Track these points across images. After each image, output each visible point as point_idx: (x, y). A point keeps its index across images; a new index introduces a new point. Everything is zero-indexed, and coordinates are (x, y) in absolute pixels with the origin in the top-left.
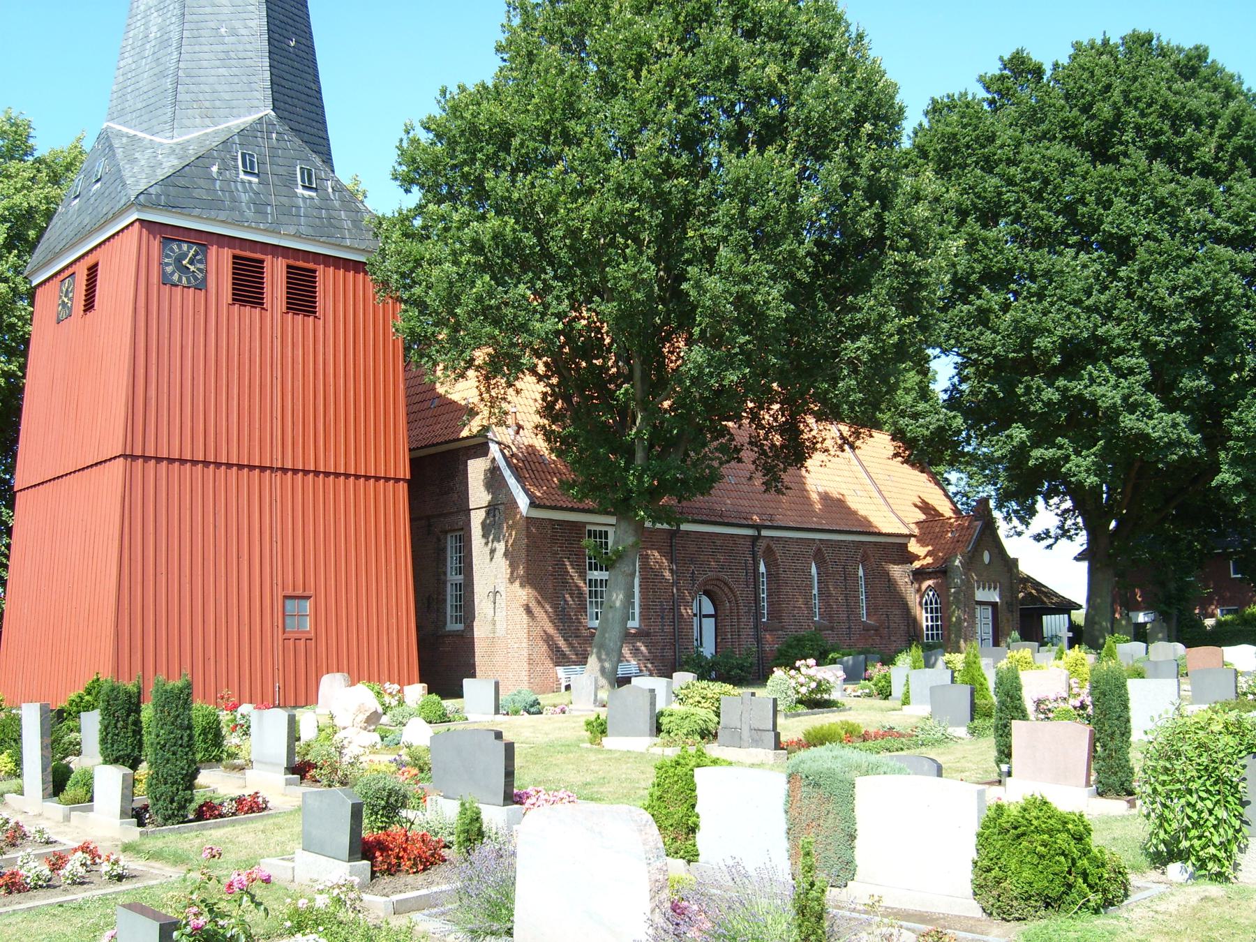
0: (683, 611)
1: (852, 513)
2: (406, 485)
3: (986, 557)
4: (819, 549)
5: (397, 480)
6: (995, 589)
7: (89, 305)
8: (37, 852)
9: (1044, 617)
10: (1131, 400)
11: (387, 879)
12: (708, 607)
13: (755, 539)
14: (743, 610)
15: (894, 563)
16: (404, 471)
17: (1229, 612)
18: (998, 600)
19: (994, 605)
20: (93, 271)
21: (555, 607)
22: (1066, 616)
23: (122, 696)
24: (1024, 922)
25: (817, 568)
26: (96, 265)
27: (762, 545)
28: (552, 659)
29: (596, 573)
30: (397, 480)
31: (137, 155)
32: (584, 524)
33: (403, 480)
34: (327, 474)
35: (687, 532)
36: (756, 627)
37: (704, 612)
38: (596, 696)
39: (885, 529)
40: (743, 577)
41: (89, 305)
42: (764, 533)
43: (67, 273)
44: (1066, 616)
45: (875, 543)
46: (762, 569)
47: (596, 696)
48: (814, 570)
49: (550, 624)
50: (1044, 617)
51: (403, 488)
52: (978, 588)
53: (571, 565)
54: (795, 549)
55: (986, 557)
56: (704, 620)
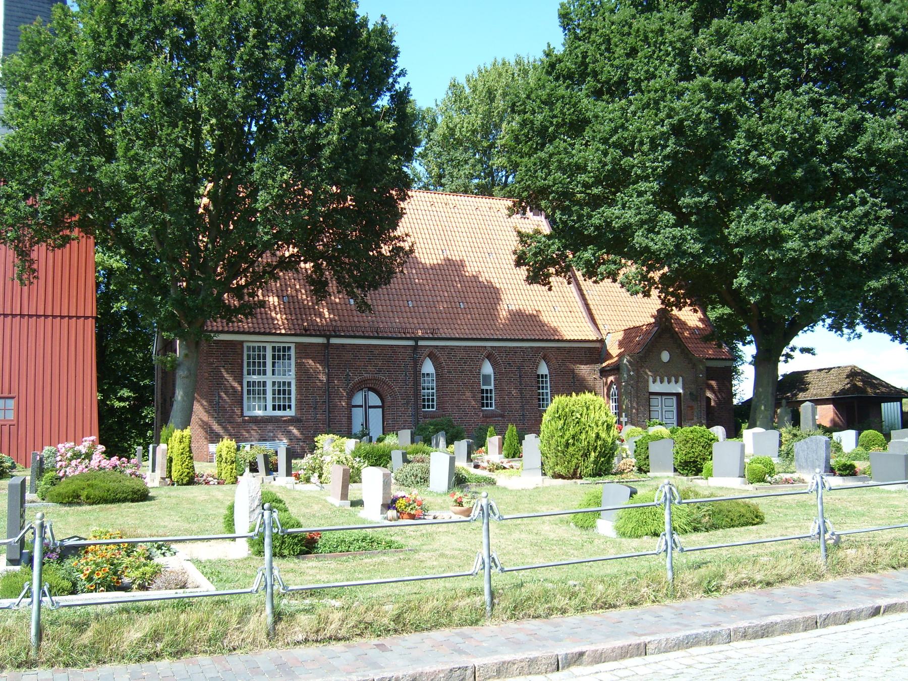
0: (117, 404)
1: (542, 325)
2: (94, 320)
5: (86, 318)
6: (676, 382)
9: (882, 404)
10: (819, 146)
12: (374, 399)
13: (416, 347)
15: (581, 363)
16: (91, 309)
17: (647, 374)
18: (681, 391)
19: (678, 395)
21: (210, 402)
22: (899, 403)
23: (760, 418)
28: (206, 438)
29: (254, 377)
30: (86, 318)
32: (242, 342)
33: (92, 317)
34: (30, 316)
39: (568, 336)
44: (899, 403)
45: (558, 348)
49: (205, 414)
50: (882, 404)
51: (90, 324)
52: (654, 382)
53: (227, 371)
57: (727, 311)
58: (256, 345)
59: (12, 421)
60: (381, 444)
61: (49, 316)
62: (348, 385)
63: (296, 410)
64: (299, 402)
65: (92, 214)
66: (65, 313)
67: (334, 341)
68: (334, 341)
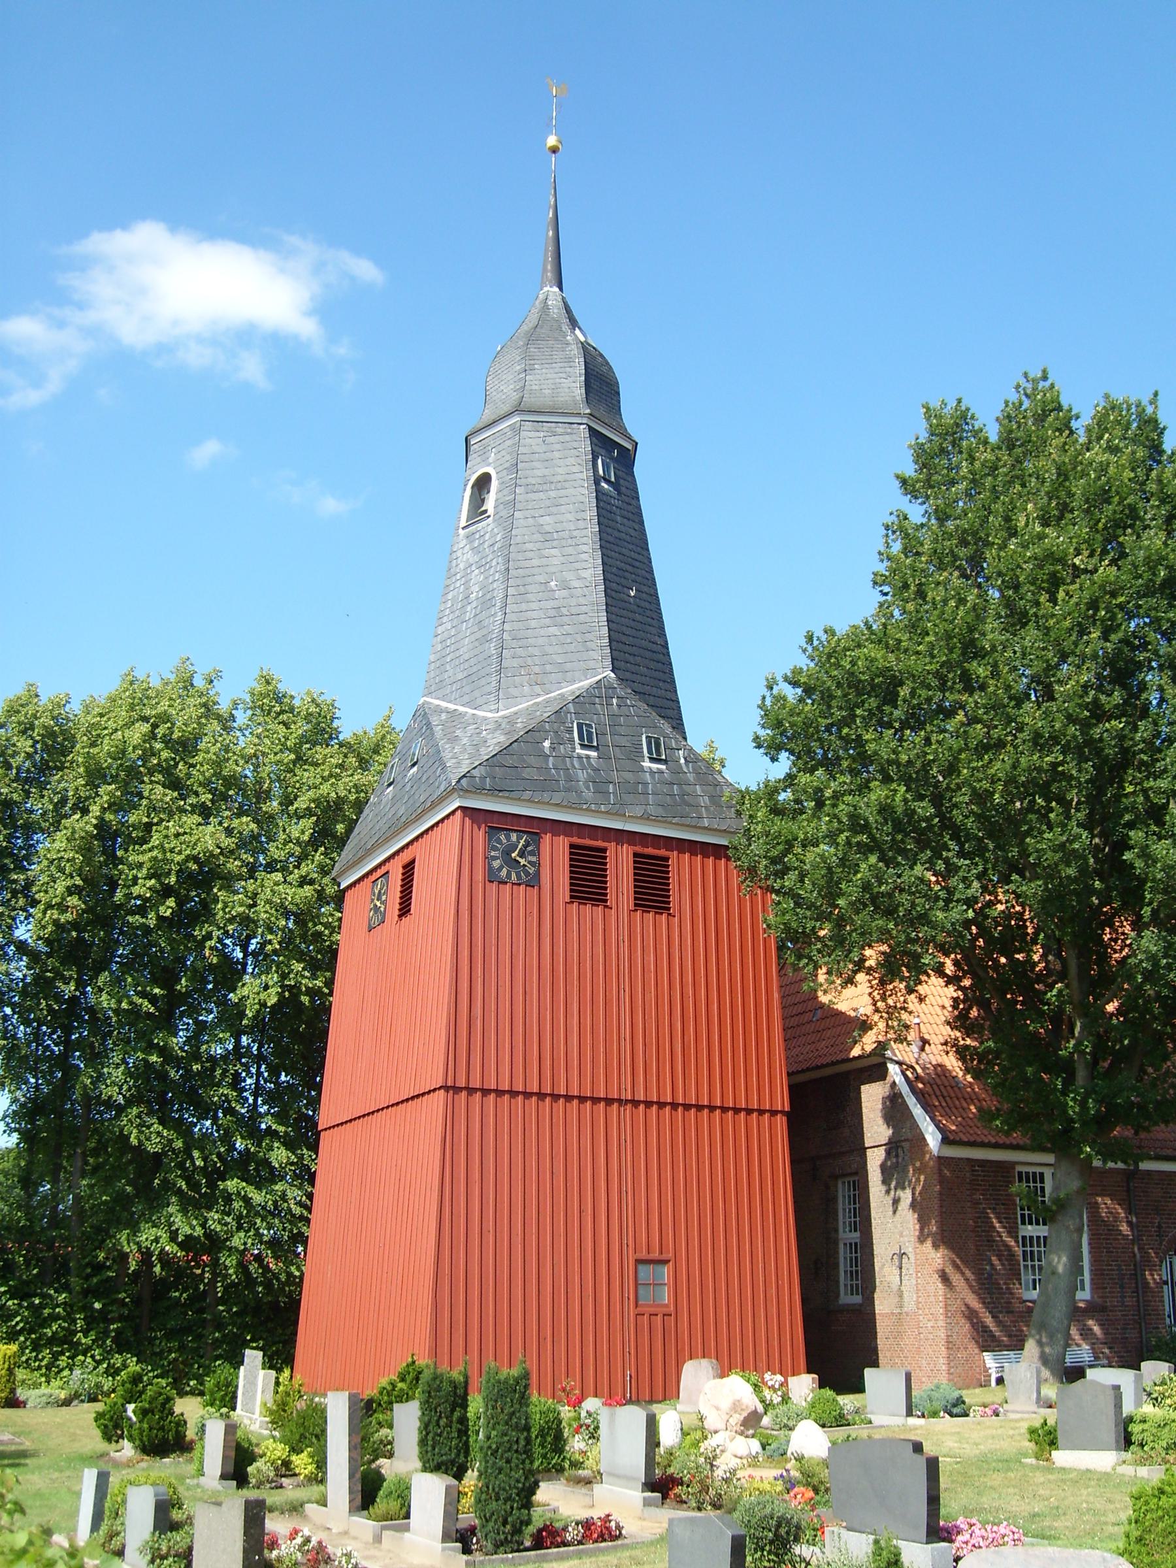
2: (785, 1119)
5: (773, 1113)
16: (782, 1101)
21: (979, 1273)
30: (773, 1113)
32: (1013, 1164)
33: (781, 1112)
51: (781, 1122)
57: (856, 1052)
58: (1031, 1169)
59: (666, 1306)
60: (118, 1454)
61: (461, 1089)
62: (1160, 1244)
63: (1092, 1289)
64: (1097, 1273)
65: (1119, 1011)
66: (462, 1083)
67: (1145, 1166)
68: (1145, 1166)
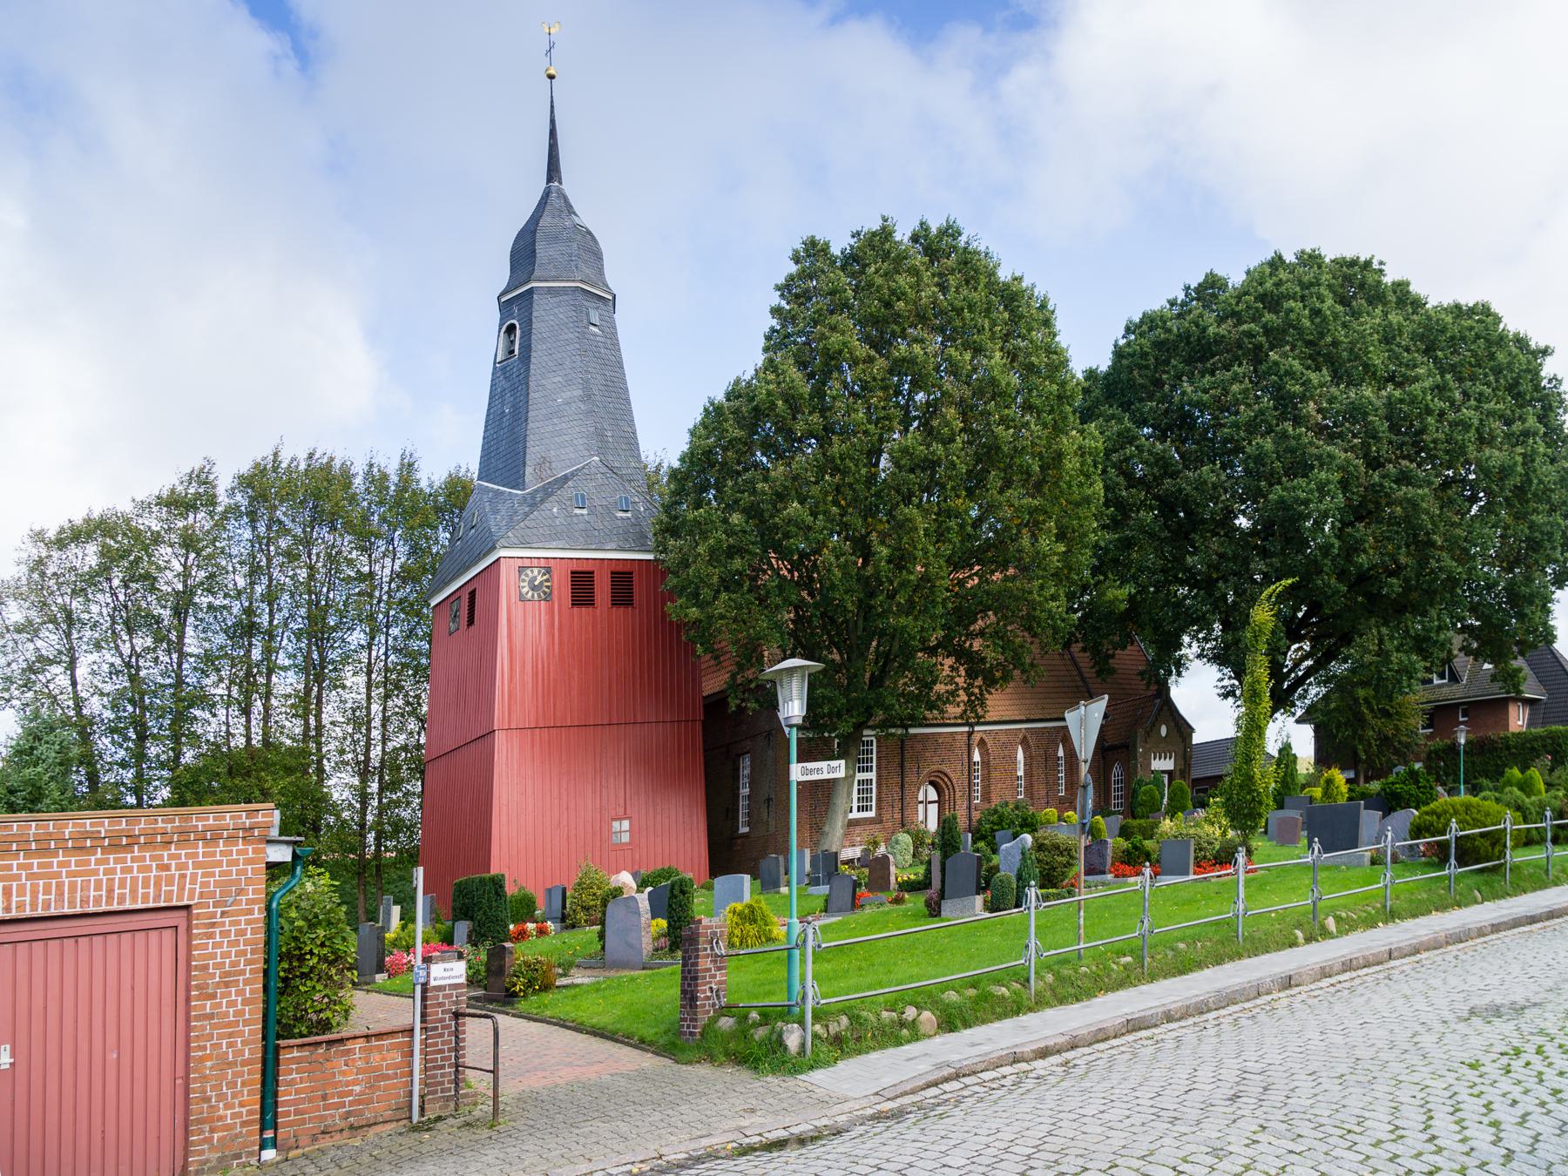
3: (1164, 731)
4: (1025, 737)
7: (471, 622)
8: (472, 994)
11: (1304, 853)
12: (933, 794)
14: (958, 794)
20: (472, 594)
24: (1479, 1001)
25: (1024, 753)
26: (474, 591)
27: (976, 738)
31: (500, 507)
35: (915, 735)
36: (969, 808)
37: (929, 799)
38: (275, 1134)
40: (959, 767)
41: (471, 622)
42: (977, 728)
43: (456, 596)
46: (977, 757)
47: (275, 1134)
48: (1020, 755)
54: (1003, 738)
55: (1164, 731)
56: (929, 806)
